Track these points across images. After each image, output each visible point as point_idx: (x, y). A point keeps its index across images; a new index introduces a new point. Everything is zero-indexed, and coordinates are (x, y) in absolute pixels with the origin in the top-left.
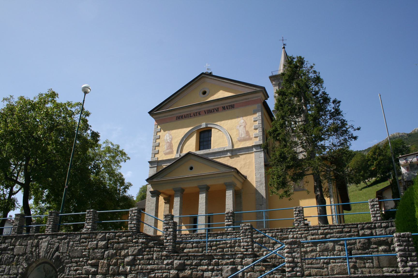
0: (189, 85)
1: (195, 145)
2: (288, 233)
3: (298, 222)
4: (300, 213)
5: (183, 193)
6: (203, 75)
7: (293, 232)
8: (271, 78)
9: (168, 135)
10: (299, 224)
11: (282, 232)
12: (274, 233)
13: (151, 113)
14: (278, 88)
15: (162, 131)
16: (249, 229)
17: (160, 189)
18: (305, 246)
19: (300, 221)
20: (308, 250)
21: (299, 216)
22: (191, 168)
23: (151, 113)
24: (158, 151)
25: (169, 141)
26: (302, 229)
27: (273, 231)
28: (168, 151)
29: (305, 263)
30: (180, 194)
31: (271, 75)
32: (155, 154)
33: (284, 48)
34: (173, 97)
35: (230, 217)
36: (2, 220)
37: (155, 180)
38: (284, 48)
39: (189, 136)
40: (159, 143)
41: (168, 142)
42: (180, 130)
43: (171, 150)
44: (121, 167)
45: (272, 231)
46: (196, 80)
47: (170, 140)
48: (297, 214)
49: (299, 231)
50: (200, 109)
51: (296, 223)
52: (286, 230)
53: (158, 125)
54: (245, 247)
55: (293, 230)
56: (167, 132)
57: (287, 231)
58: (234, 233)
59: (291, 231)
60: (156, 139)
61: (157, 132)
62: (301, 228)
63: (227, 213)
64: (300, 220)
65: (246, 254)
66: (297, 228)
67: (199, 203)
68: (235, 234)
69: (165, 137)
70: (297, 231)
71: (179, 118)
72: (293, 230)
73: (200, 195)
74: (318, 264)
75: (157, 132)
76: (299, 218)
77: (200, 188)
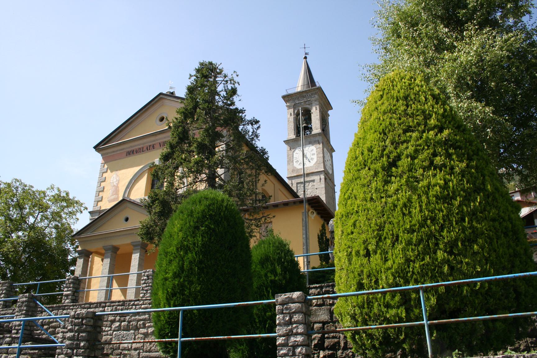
0: (144, 110)
1: (144, 188)
2: (130, 307)
3: (145, 292)
4: (148, 279)
5: (116, 253)
6: (161, 96)
7: (136, 305)
8: (284, 97)
9: (115, 176)
10: (145, 294)
11: (124, 306)
12: (114, 307)
13: (97, 148)
14: (293, 111)
15: (109, 171)
16: (25, 301)
17: (91, 247)
18: (147, 325)
19: (147, 290)
20: (149, 332)
21: (146, 284)
22: (127, 219)
23: (97, 148)
24: (102, 197)
25: (115, 184)
26: (147, 301)
27: (114, 304)
28: (113, 197)
29: (143, 351)
30: (110, 253)
31: (285, 93)
32: (98, 201)
33: (306, 58)
34: (124, 126)
35: (70, 284)
36: (442, 290)
37: (83, 236)
38: (306, 58)
39: (139, 177)
40: (104, 187)
41: (114, 186)
42: (135, 168)
43: (117, 196)
44: (78, 219)
45: (112, 304)
46: (153, 103)
47: (117, 182)
48: (145, 280)
49: (143, 304)
50: (154, 141)
51: (142, 293)
52: (128, 303)
53: (105, 163)
54: (16, 328)
55: (136, 303)
56: (114, 172)
57: (130, 303)
58: (71, 306)
59: (133, 305)
60: (101, 182)
61: (103, 173)
62: (146, 300)
63: (68, 279)
64: (147, 288)
65: (15, 338)
66: (141, 300)
67: (132, 265)
68: (71, 307)
69: (112, 179)
70: (141, 305)
71: (130, 153)
72: (136, 303)
73: (133, 255)
74: (157, 352)
75: (103, 173)
76: (146, 287)
77: (134, 246)
